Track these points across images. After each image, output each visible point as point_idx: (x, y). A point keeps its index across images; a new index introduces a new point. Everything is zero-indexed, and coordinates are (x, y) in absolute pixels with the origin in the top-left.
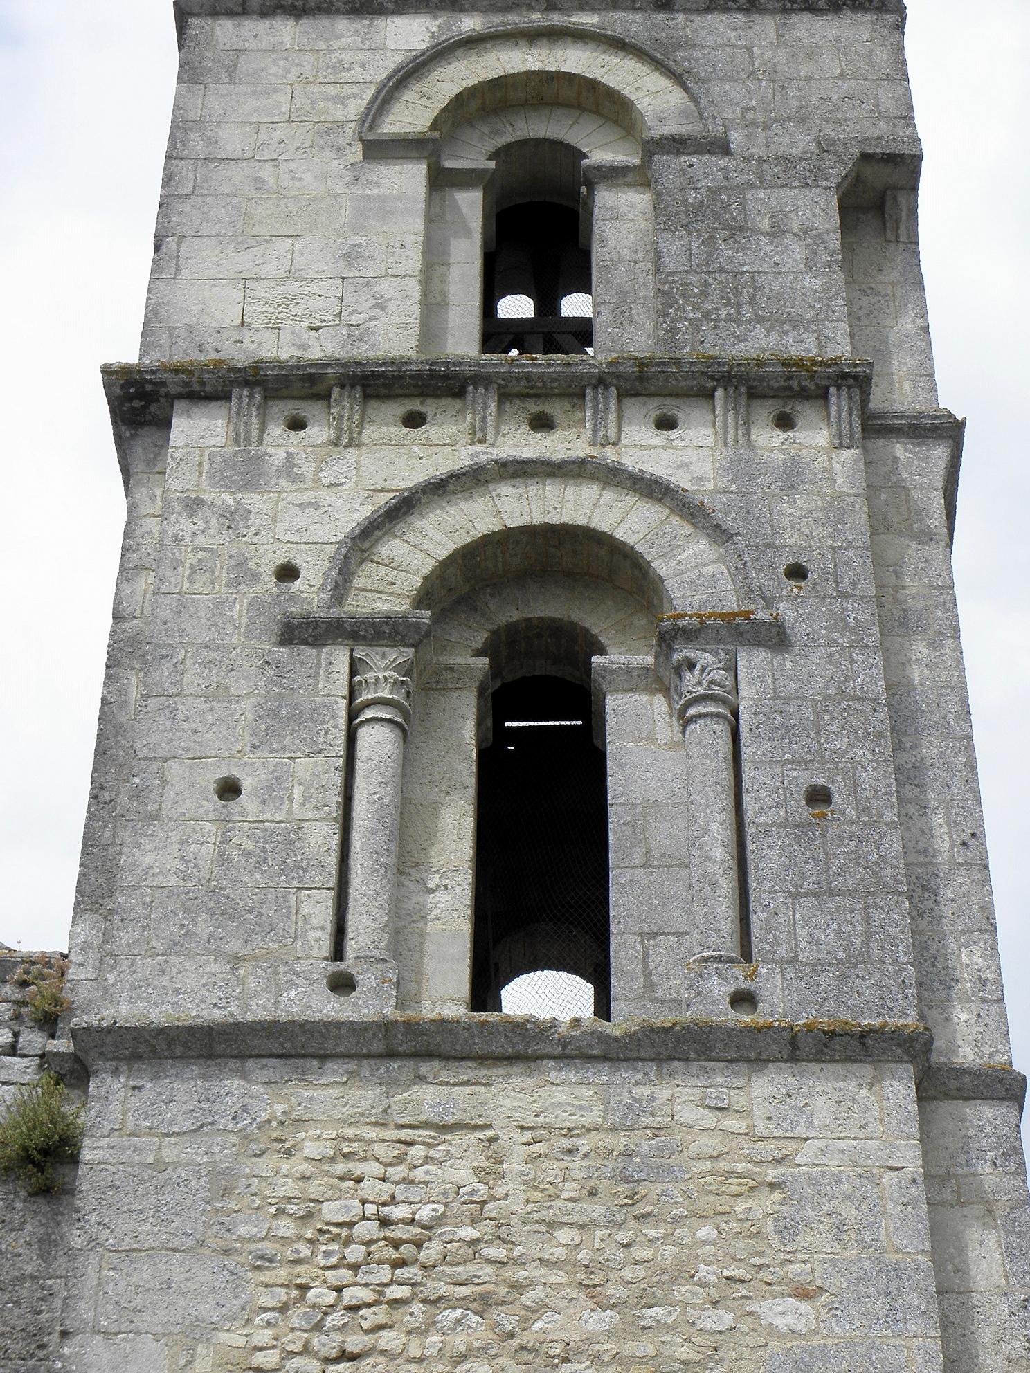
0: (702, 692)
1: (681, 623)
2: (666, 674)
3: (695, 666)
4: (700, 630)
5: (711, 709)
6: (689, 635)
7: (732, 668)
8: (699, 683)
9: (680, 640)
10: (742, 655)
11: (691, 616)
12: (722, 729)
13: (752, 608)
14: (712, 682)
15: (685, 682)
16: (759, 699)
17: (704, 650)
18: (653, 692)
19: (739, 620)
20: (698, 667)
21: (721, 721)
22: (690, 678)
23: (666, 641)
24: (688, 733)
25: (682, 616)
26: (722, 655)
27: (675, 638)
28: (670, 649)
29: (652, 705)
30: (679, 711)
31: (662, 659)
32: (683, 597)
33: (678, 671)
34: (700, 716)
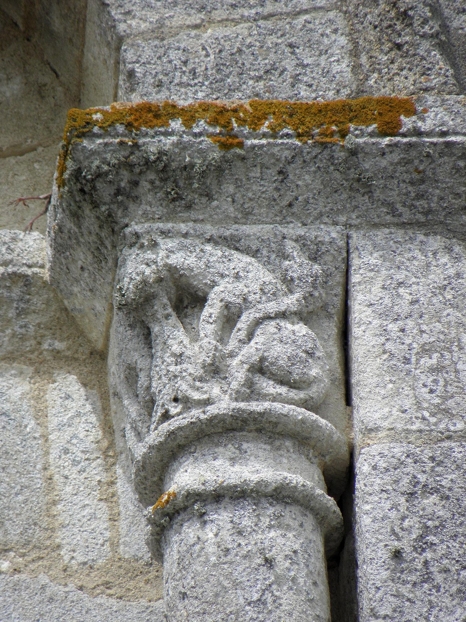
0: (224, 406)
1: (154, 144)
2: (94, 309)
3: (200, 301)
4: (220, 170)
5: (256, 468)
6: (181, 186)
7: (332, 312)
8: (215, 370)
9: (150, 201)
10: (367, 262)
11: (189, 116)
12: (294, 544)
13: (403, 85)
14: (260, 368)
15: (164, 363)
16: (429, 437)
17: (233, 243)
18: (42, 366)
19: (361, 136)
20: (212, 310)
21: (291, 515)
22: (184, 346)
23: (97, 203)
24: (173, 552)
25: (155, 115)
26: (298, 265)
27: (127, 195)
28: (111, 238)
29: (40, 415)
30: (143, 466)
31: (82, 256)
32: (159, 32)
33: (139, 313)
34: (220, 496)
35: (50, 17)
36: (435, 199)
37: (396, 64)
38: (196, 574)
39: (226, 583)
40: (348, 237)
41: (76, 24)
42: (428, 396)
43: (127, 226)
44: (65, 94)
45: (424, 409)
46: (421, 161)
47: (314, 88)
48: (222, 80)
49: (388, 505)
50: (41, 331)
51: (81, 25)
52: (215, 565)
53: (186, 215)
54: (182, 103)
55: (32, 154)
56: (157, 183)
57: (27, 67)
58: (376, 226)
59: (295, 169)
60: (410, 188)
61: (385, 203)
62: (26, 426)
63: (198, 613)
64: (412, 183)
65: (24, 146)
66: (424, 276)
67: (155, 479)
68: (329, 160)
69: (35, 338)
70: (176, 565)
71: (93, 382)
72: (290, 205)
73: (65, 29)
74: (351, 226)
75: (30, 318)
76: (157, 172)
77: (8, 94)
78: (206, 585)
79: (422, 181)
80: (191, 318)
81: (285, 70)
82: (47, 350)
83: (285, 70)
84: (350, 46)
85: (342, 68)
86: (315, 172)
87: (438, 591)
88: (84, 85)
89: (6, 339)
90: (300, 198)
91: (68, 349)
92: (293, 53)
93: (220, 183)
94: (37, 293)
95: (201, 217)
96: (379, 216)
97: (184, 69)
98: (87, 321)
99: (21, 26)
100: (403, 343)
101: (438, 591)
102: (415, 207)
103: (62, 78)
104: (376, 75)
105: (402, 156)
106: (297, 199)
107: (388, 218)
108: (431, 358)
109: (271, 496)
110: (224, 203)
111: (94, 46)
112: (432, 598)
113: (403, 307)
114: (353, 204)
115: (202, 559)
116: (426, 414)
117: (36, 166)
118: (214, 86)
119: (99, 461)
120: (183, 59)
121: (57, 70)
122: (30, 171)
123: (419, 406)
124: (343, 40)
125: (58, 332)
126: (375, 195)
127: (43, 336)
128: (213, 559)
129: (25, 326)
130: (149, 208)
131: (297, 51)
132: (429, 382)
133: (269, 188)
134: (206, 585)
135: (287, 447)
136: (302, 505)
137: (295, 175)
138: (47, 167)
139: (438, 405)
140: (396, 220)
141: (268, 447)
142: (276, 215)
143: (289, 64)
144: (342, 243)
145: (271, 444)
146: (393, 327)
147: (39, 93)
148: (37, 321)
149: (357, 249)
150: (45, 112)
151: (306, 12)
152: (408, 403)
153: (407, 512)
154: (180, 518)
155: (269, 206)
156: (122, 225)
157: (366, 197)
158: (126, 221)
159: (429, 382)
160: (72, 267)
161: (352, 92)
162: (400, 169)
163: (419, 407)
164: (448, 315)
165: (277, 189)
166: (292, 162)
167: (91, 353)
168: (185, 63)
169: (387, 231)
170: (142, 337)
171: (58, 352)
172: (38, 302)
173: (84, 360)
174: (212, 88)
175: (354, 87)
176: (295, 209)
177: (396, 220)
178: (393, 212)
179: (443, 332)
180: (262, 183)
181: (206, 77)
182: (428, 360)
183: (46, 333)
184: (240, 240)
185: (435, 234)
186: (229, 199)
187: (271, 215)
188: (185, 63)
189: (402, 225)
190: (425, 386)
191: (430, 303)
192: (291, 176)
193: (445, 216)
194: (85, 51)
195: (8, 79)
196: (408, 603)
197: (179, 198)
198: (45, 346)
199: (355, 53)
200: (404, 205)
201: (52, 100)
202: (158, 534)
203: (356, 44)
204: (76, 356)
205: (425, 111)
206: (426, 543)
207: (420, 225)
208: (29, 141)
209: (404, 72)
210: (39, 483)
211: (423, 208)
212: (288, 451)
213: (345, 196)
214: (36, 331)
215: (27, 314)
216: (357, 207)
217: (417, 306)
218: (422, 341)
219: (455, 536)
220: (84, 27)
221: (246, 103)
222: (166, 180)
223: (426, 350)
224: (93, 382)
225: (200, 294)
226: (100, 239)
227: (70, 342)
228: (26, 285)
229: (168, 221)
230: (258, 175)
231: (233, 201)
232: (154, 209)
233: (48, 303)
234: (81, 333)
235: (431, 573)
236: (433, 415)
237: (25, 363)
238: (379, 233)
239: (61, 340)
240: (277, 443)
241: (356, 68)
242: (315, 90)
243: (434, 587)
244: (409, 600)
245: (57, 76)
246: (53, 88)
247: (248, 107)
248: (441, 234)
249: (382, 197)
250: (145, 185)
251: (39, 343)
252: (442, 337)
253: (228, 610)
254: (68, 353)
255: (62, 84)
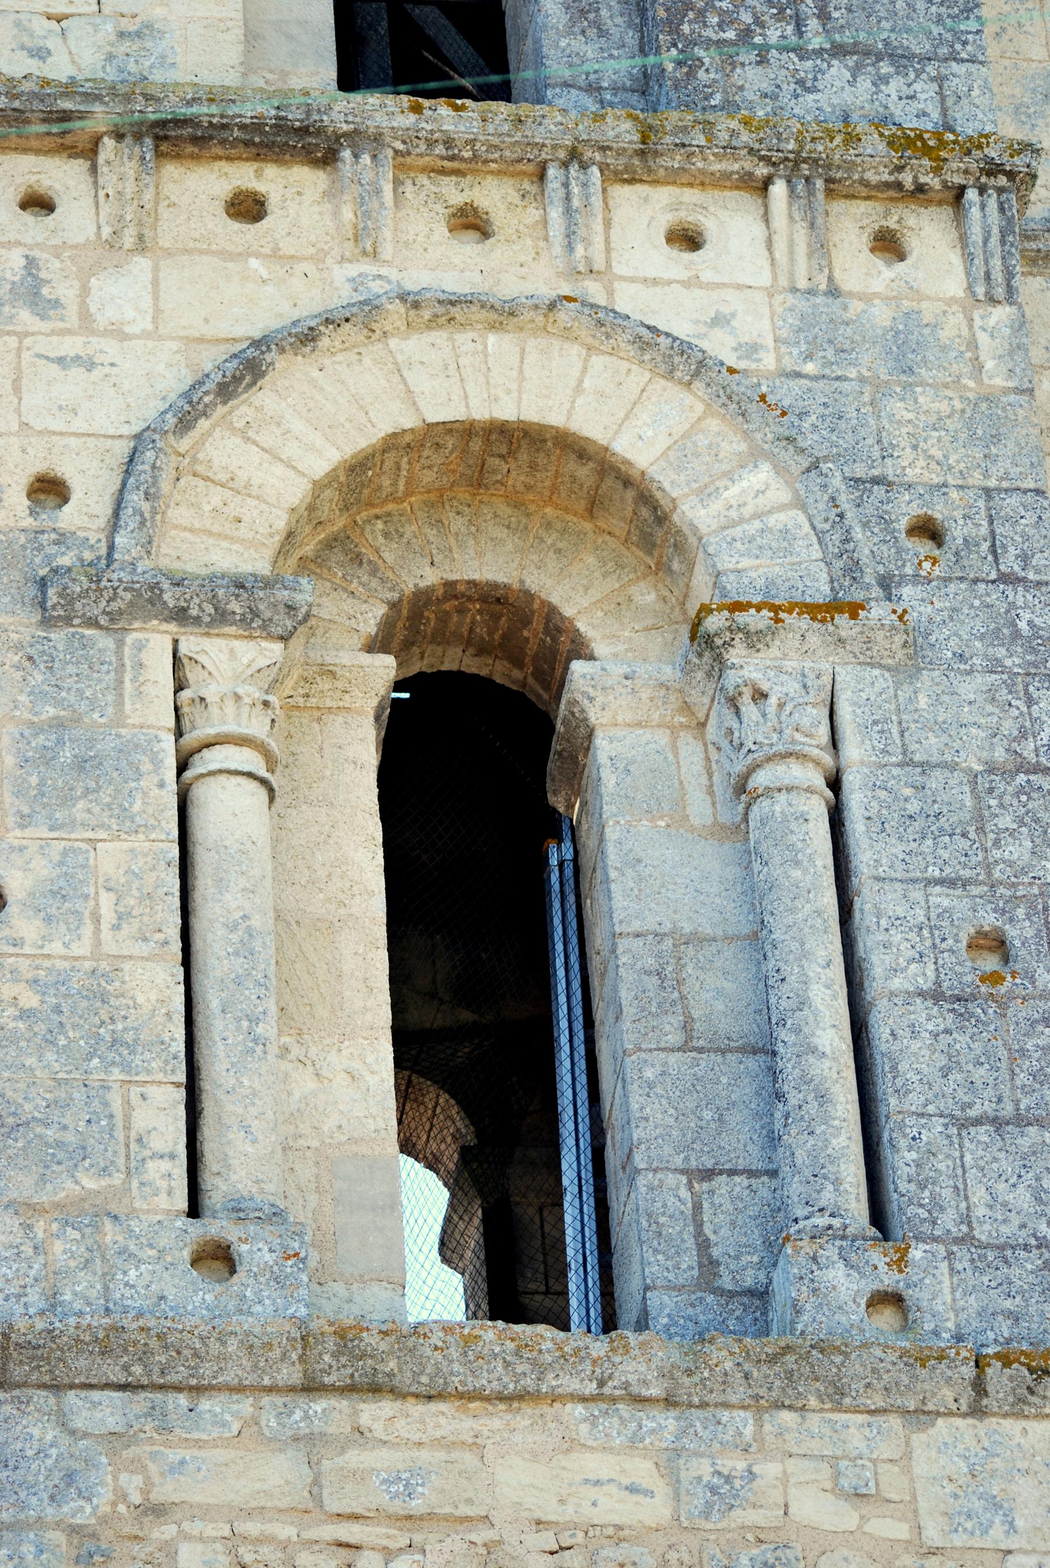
3: (765, 696)
54: (754, 602)
113: (863, 702)
133: (797, 644)
143: (801, 586)
146: (859, 711)
152: (869, 748)
178: (855, 657)
210: (677, 785)
219: (70, 1477)
223: (875, 723)
241: (832, 589)
250: (737, 640)
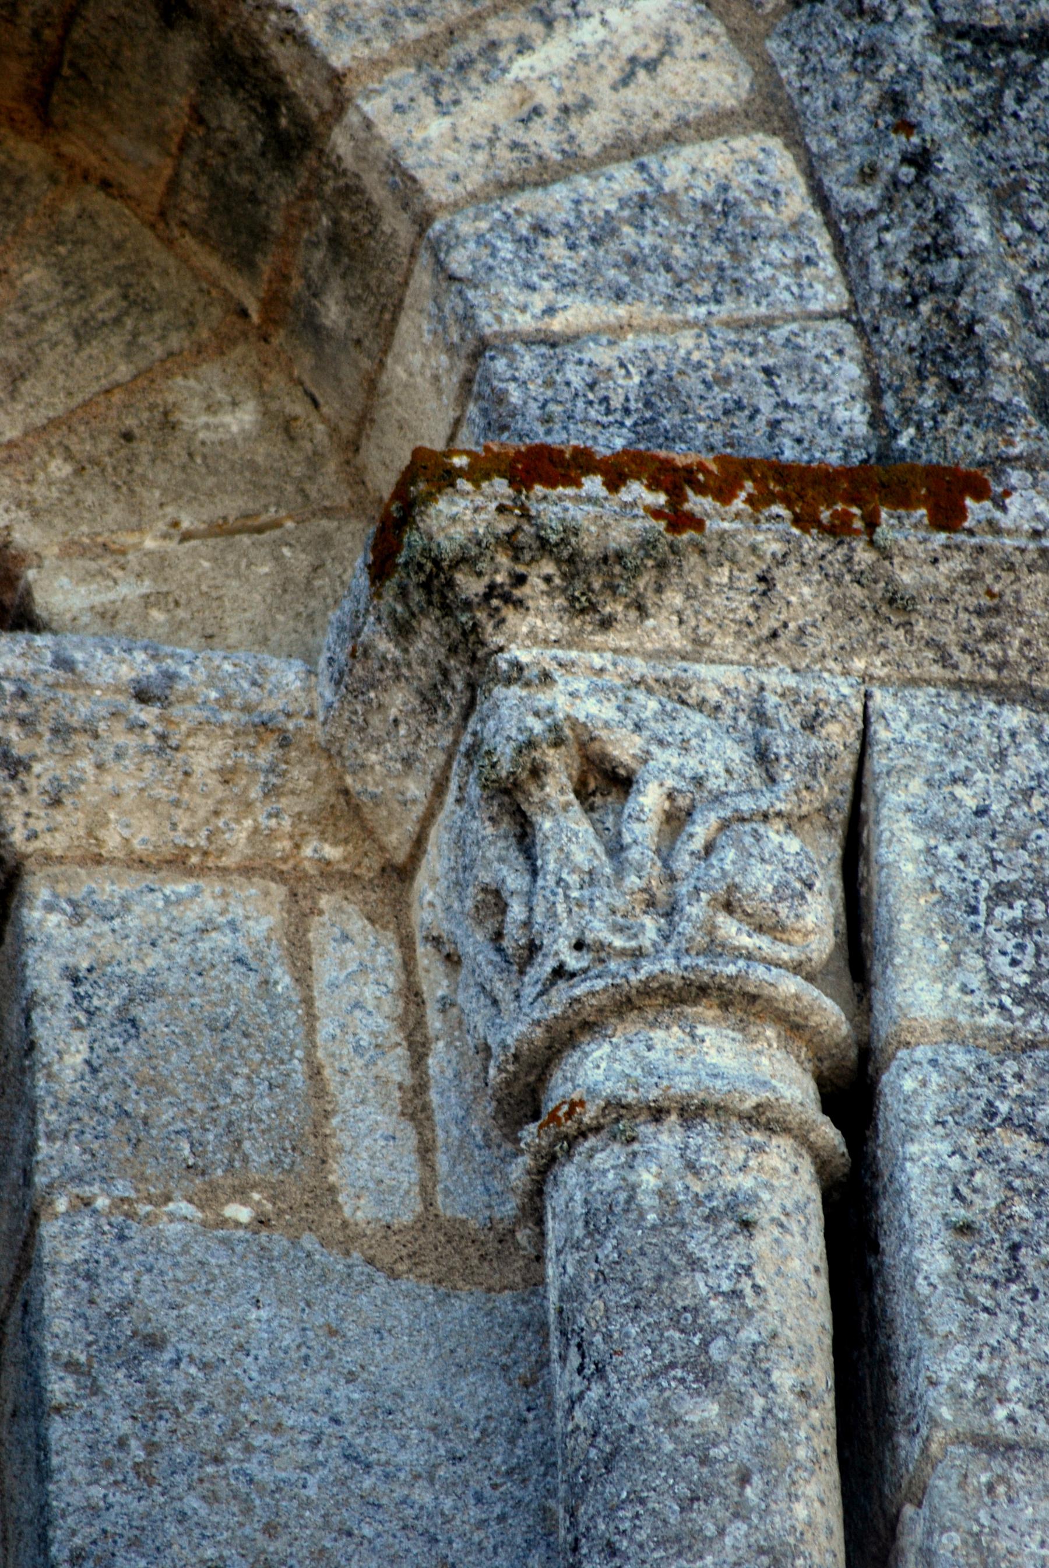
35: (323, 303)
36: (1016, 643)
37: (951, 414)
38: (621, 1239)
39: (674, 1259)
40: (868, 696)
41: (376, 314)
42: (1008, 971)
43: (501, 649)
44: (331, 437)
45: (1001, 991)
46: (998, 578)
47: (806, 444)
48: (653, 420)
49: (945, 1147)
50: (302, 826)
51: (387, 316)
52: (654, 1227)
53: (599, 639)
54: (602, 451)
55: (277, 533)
56: (557, 581)
57: (265, 387)
58: (914, 682)
59: (786, 575)
60: (975, 622)
61: (930, 643)
62: (276, 983)
63: (627, 1307)
64: (979, 612)
65: (264, 518)
66: (997, 771)
67: (532, 1079)
68: (844, 563)
69: (291, 837)
70: (581, 1224)
71: (387, 918)
72: (774, 635)
73: (350, 323)
74: (871, 678)
75: (284, 801)
76: (558, 561)
77: (235, 429)
78: (639, 1260)
79: (996, 611)
80: (601, 811)
81: (757, 411)
82: (310, 859)
83: (757, 411)
84: (865, 382)
85: (854, 417)
86: (819, 583)
87: (1034, 1298)
88: (372, 421)
89: (244, 835)
90: (792, 625)
91: (345, 859)
92: (771, 384)
93: (659, 590)
94: (300, 761)
95: (625, 644)
96: (919, 665)
97: (591, 396)
98: (385, 813)
99: (255, 318)
100: (964, 880)
101: (1034, 1298)
102: (982, 656)
103: (325, 410)
104: (912, 431)
105: (966, 566)
106: (785, 625)
107: (936, 670)
108: (1011, 907)
109: (749, 1118)
110: (666, 623)
111: (414, 351)
112: (1026, 1309)
114: (880, 640)
115: (633, 1216)
116: (1007, 1001)
117: (286, 551)
118: (640, 429)
119: (399, 1051)
120: (589, 379)
121: (317, 395)
122: (276, 559)
123: (993, 983)
124: (853, 370)
125: (331, 829)
126: (916, 629)
127: (304, 835)
128: (651, 1217)
129: (277, 815)
130: (539, 623)
131: (778, 381)
132: (1009, 947)
134: (639, 1260)
135: (768, 1040)
136: (795, 1137)
137: (787, 585)
138: (303, 556)
139: (1026, 989)
140: (948, 674)
141: (739, 1036)
142: (749, 651)
144: (858, 707)
145: (743, 1030)
146: (948, 852)
147: (287, 430)
148: (297, 809)
149: (883, 716)
150: (297, 463)
151: (794, 319)
152: (976, 981)
153: (978, 1161)
154: (587, 1145)
155: (738, 634)
156: (492, 647)
157: (901, 632)
158: (500, 640)
159: (1009, 947)
160: (375, 720)
161: (869, 455)
162: (962, 587)
163: (994, 989)
164: (1039, 837)
165: (755, 607)
166: (783, 564)
167: (383, 870)
168: (592, 386)
169: (932, 691)
170: (512, 840)
171: (328, 863)
172: (299, 776)
173: (371, 881)
174: (637, 433)
175: (873, 449)
176: (781, 643)
177: (948, 674)
178: (944, 659)
179: (1030, 866)
180: (731, 594)
181: (627, 411)
182: (1007, 911)
183: (311, 830)
184: (690, 687)
185: (1014, 702)
186: (675, 618)
187: (741, 650)
188: (592, 386)
189: (957, 685)
190: (1004, 953)
191: (1008, 816)
192: (779, 587)
193: (1030, 673)
194: (389, 361)
195: (235, 404)
196: (984, 1316)
197: (593, 607)
198: (308, 851)
199: (875, 392)
200: (964, 648)
201: (308, 446)
202: (539, 1172)
203: (875, 379)
204: (357, 871)
205: (1007, 493)
206: (1011, 1217)
207: (989, 687)
208: (273, 509)
209: (966, 428)
210: (299, 1079)
211: (995, 657)
212: (770, 1046)
213: (865, 626)
214: (293, 825)
215: (279, 795)
216: (884, 646)
217: (985, 819)
218: (995, 878)
220: (395, 320)
221: (709, 460)
222: (573, 577)
223: (1003, 894)
224: (387, 918)
225: (622, 772)
226: (445, 673)
227: (350, 848)
228: (281, 746)
229: (570, 646)
230: (725, 580)
231: (681, 622)
232: (548, 625)
233: (316, 779)
234: (369, 833)
235: (1023, 1267)
236: (1018, 1003)
237: (273, 879)
238: (919, 693)
239: (335, 844)
240: (753, 1030)
241: (877, 419)
242: (808, 449)
243: (1027, 1290)
244: (986, 1309)
245: (316, 404)
246: (310, 425)
247: (714, 467)
248: (1023, 703)
249: (927, 633)
250: (534, 583)
251: (297, 846)
252: (1030, 874)
253: (680, 1304)
254: (346, 867)
255: (325, 420)
